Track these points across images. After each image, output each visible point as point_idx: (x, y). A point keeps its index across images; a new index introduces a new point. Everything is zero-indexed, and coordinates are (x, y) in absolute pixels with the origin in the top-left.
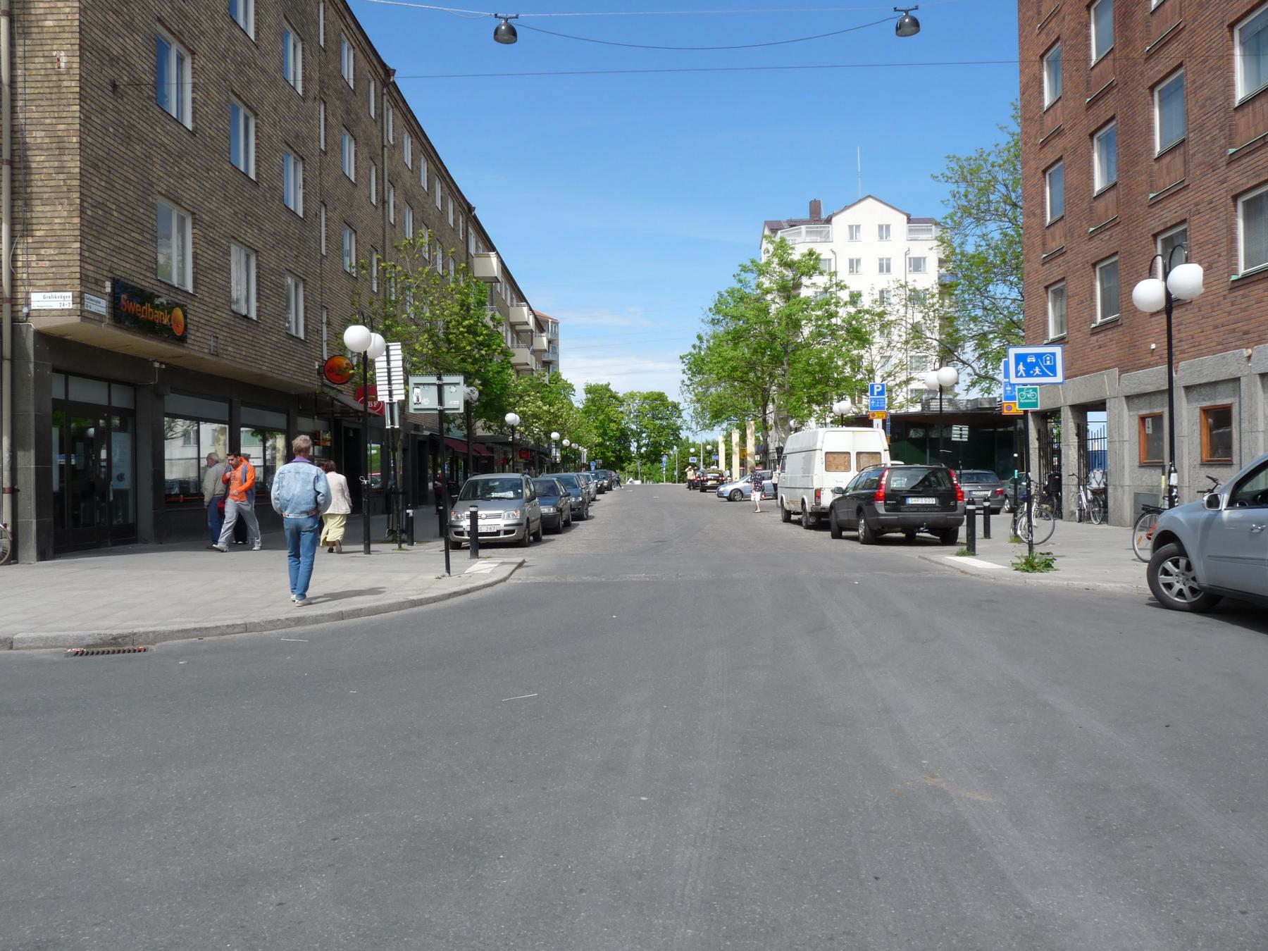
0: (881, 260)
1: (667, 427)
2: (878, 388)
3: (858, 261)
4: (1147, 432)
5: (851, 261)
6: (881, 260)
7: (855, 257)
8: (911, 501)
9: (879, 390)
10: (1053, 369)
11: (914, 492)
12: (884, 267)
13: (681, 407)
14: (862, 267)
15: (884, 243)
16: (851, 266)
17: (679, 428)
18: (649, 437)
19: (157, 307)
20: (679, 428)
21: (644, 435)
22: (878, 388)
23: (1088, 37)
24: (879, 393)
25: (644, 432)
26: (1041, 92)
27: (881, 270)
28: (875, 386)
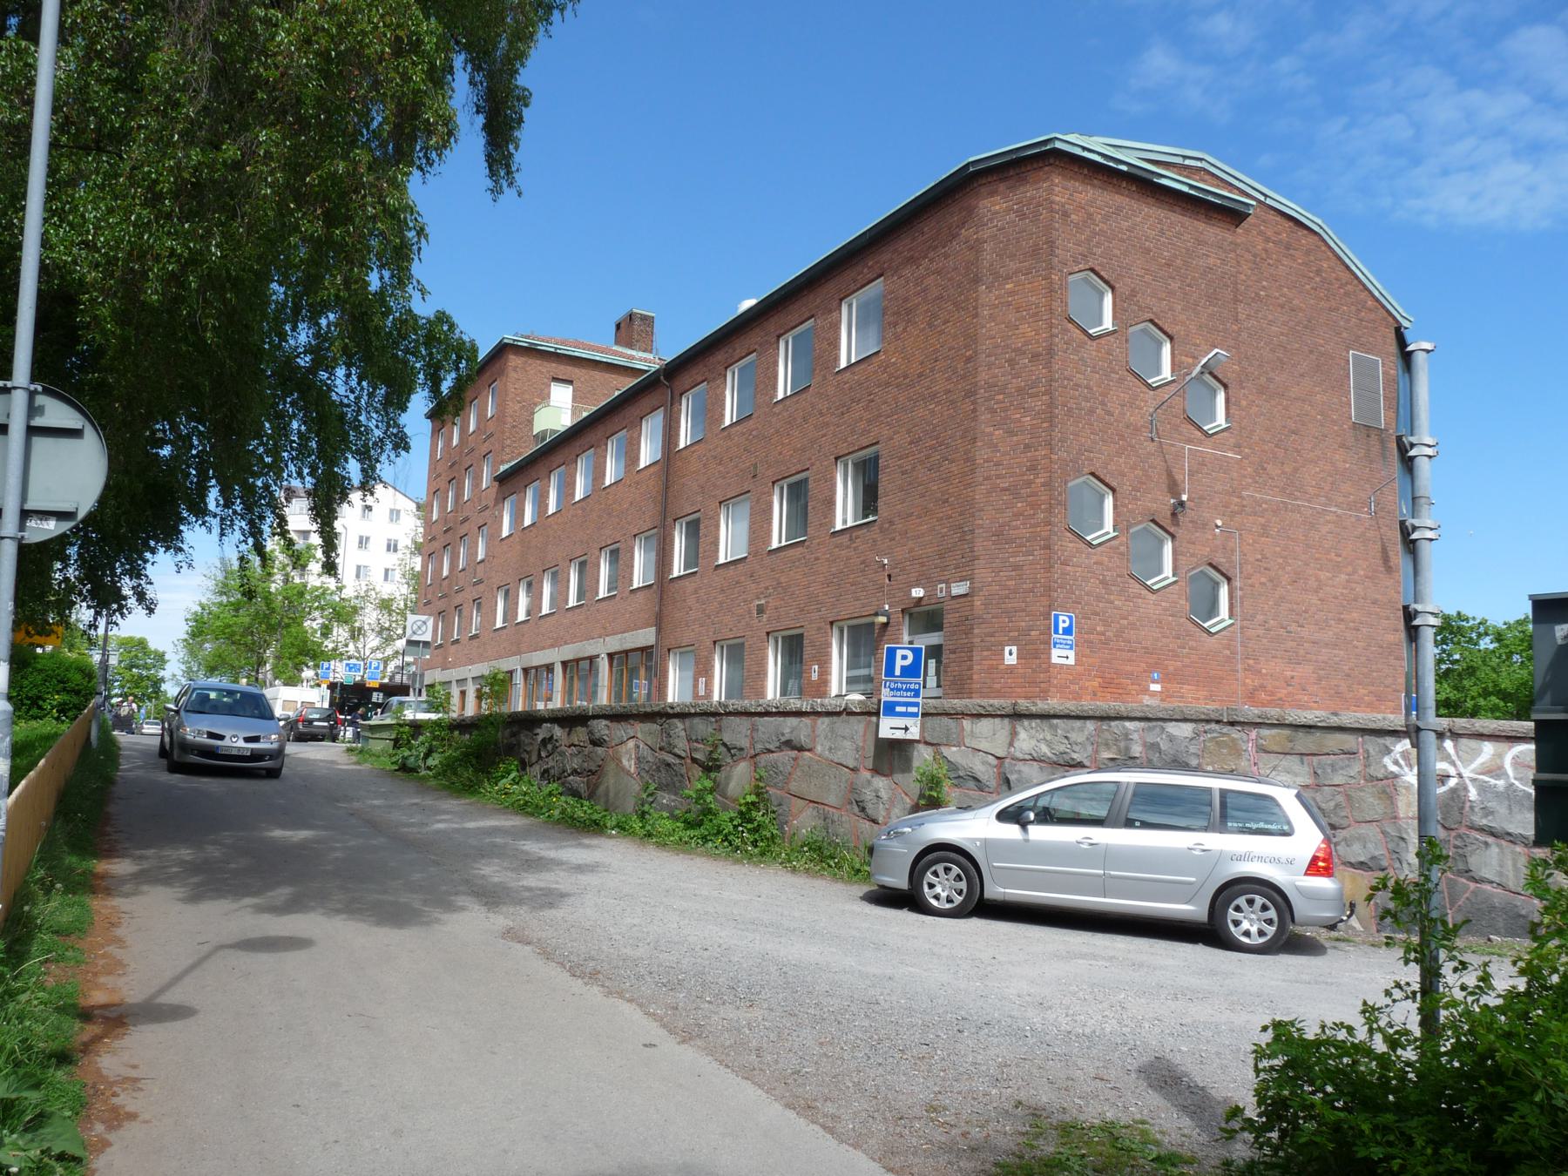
0: (389, 540)
1: (148, 677)
2: (904, 657)
3: (368, 539)
4: (375, 694)
5: (361, 538)
6: (389, 540)
7: (365, 534)
8: (316, 723)
9: (909, 661)
10: (359, 670)
11: (319, 720)
12: (392, 547)
13: (167, 657)
14: (371, 545)
15: (393, 526)
16: (361, 542)
17: (162, 680)
18: (122, 687)
19: (539, 751)
20: (162, 680)
21: (116, 684)
22: (904, 657)
23: (448, 497)
24: (375, 668)
25: (117, 681)
26: (432, 512)
27: (389, 550)
28: (899, 653)
